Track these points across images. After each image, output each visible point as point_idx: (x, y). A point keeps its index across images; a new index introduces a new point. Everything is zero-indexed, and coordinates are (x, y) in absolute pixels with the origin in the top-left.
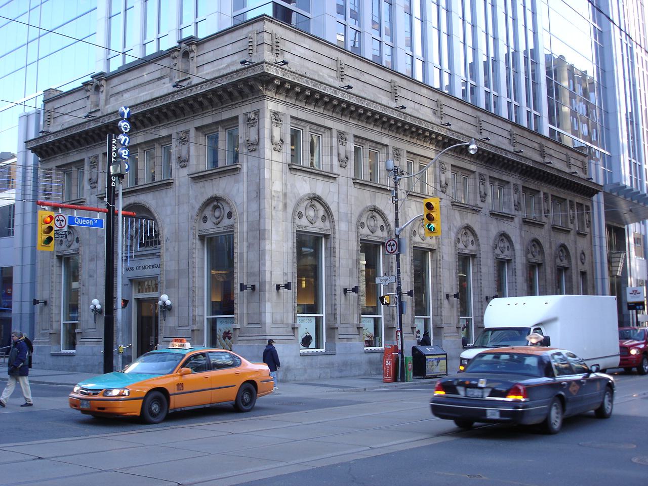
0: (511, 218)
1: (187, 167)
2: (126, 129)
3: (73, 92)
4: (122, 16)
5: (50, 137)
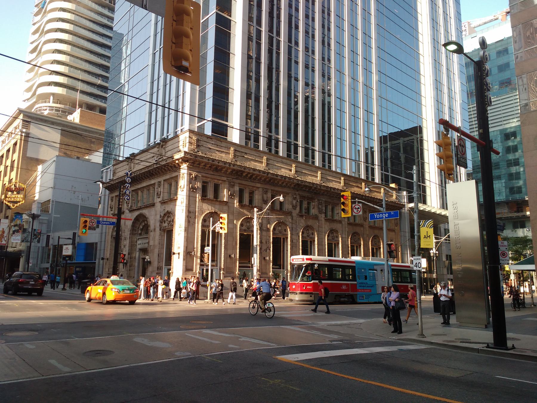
2: (129, 181)
4: (124, 134)
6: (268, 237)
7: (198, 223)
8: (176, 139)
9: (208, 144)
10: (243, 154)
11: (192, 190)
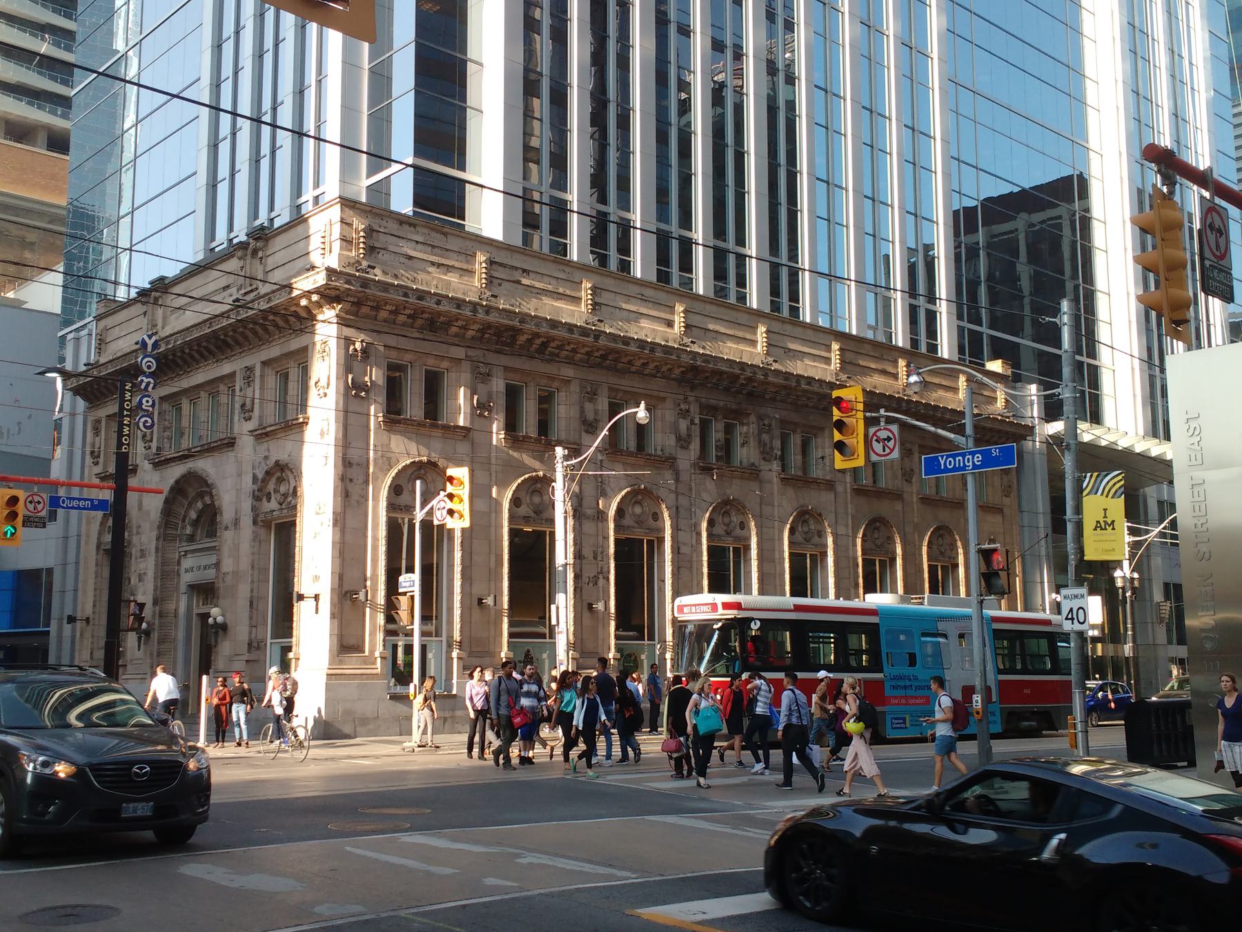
2: (149, 367)
7: (376, 499)
10: (517, 275)
11: (354, 393)
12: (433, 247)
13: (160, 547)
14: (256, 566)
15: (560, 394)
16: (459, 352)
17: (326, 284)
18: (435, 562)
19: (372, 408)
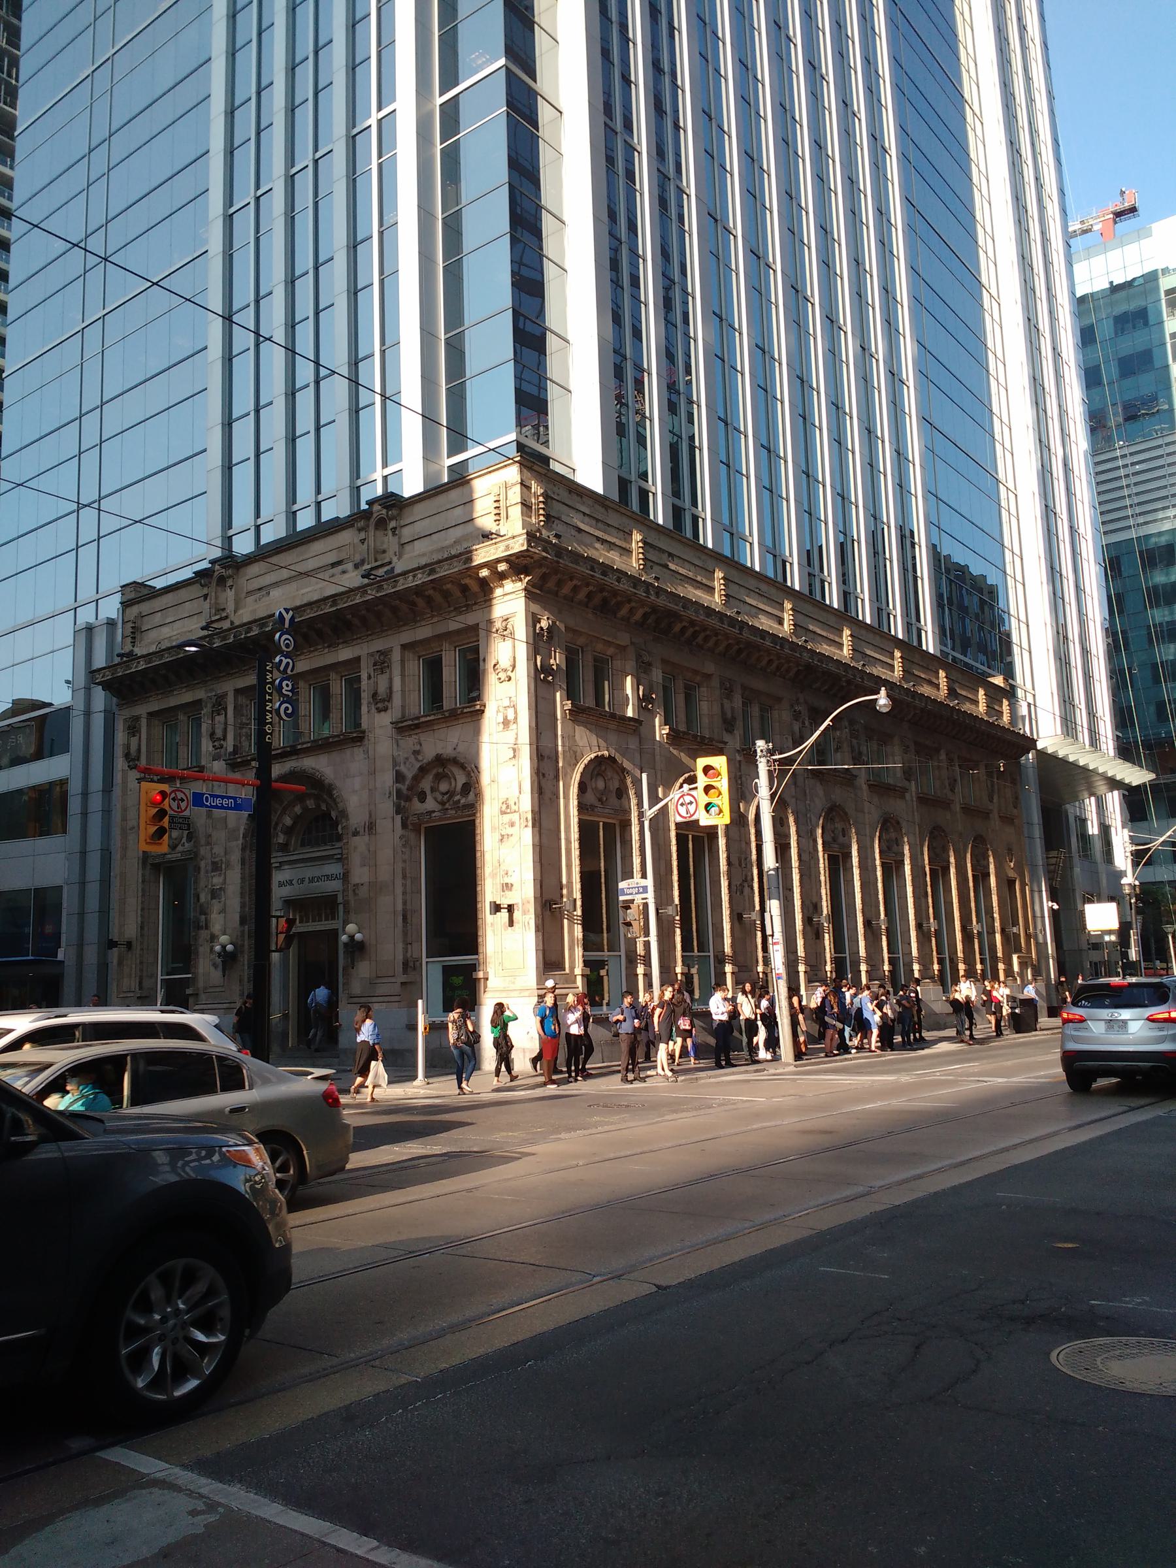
0: (901, 793)
1: (389, 711)
2: (287, 646)
3: (178, 589)
5: (139, 663)
6: (744, 845)
7: (566, 797)
8: (454, 495)
9: (572, 514)
10: (664, 558)
11: (541, 678)
12: (597, 520)
13: (247, 857)
14: (408, 875)
15: (701, 689)
16: (624, 639)
17: (527, 550)
18: (603, 869)
19: (558, 694)
